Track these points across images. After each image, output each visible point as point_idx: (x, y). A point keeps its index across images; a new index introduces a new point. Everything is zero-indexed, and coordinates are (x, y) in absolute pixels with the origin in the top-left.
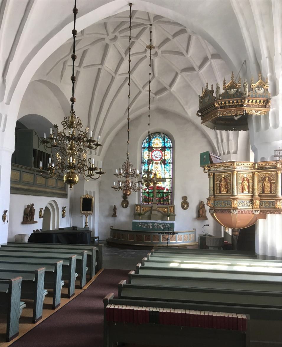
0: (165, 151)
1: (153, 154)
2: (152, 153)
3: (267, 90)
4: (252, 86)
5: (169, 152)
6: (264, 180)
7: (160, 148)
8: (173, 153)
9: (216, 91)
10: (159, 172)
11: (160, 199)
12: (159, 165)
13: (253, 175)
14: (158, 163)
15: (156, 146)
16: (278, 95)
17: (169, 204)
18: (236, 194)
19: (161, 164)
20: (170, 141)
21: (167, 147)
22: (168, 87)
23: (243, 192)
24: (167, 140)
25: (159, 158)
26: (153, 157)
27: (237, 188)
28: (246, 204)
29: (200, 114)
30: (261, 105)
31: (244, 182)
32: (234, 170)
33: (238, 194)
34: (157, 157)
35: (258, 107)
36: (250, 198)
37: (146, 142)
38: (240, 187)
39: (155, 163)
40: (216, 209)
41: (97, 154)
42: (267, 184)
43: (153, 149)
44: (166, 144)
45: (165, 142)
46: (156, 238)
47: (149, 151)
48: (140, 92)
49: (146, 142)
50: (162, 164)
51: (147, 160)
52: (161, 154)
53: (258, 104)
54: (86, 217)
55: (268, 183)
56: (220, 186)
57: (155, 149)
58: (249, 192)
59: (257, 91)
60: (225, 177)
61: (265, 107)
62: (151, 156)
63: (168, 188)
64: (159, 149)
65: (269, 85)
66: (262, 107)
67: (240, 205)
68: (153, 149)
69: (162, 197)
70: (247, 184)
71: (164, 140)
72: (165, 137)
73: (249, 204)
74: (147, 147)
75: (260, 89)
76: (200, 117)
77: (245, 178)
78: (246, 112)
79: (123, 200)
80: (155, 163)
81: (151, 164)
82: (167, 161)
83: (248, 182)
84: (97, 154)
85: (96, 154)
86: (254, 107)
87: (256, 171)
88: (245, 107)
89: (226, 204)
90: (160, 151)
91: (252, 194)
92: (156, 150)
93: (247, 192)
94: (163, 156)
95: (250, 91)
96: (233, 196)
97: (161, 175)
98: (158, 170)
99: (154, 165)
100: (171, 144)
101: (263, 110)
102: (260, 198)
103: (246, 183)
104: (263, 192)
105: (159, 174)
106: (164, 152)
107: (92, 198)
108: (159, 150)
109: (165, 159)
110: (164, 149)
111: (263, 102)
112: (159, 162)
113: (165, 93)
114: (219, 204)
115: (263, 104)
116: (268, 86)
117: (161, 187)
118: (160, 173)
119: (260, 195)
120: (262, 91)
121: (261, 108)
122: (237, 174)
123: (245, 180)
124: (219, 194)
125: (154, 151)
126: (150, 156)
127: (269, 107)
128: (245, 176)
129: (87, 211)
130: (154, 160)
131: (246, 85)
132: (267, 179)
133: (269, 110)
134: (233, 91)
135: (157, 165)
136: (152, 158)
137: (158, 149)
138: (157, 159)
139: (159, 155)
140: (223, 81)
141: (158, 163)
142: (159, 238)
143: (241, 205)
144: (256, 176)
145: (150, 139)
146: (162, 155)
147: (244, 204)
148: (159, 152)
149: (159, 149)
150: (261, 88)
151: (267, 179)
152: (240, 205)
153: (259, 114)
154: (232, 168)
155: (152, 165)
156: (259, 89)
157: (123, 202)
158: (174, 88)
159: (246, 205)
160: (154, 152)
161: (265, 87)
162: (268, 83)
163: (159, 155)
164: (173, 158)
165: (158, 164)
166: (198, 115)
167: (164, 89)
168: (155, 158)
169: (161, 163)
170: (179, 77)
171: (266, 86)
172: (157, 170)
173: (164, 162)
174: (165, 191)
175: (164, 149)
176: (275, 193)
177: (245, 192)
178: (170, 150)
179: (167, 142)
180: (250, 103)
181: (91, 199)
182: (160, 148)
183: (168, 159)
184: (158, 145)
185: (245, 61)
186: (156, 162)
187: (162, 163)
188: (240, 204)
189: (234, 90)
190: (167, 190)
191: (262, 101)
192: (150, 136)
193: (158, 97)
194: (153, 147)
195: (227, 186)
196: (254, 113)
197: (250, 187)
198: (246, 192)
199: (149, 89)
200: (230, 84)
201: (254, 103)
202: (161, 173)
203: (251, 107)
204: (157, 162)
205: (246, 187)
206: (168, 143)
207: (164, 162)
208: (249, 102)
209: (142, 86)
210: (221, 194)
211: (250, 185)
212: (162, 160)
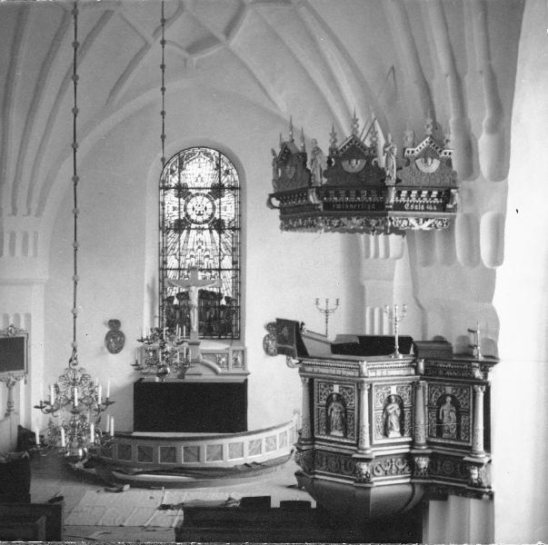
0: (220, 196)
1: (190, 206)
2: (188, 201)
3: (449, 162)
4: (406, 153)
5: (232, 200)
6: (441, 401)
7: (207, 188)
8: (240, 204)
9: (312, 161)
10: (207, 253)
11: (209, 324)
12: (206, 233)
13: (415, 385)
14: (203, 229)
15: (197, 185)
16: (440, 334)
17: (232, 336)
18: (367, 444)
19: (211, 232)
20: (235, 172)
21: (226, 185)
22: (222, 37)
23: (386, 434)
24: (225, 168)
25: (206, 217)
26: (190, 211)
27: (370, 428)
28: (394, 467)
29: (276, 202)
30: (433, 204)
31: (389, 407)
32: (363, 382)
33: (375, 442)
34: (199, 214)
35: (426, 210)
36: (405, 449)
37: (171, 173)
38: (378, 424)
39: (196, 229)
40: (317, 476)
41: (33, 213)
42: (448, 411)
43: (190, 193)
44: (223, 178)
45: (220, 172)
46: (190, 452)
47: (179, 196)
48: (147, 46)
49: (171, 173)
50: (215, 232)
51: (173, 222)
52: (209, 205)
53: (425, 200)
54: (10, 389)
55: (451, 411)
56: (327, 414)
57: (194, 192)
58: (402, 432)
59: (423, 168)
60: (341, 393)
61: (442, 208)
62: (185, 209)
63: (230, 295)
64: (206, 192)
65: (453, 150)
66: (435, 208)
67: (378, 471)
68: (190, 190)
69: (215, 318)
70: (398, 412)
71: (218, 167)
72: (220, 159)
73: (401, 467)
74: (173, 185)
75: (430, 161)
76: (277, 212)
77: (393, 397)
78: (392, 225)
79: (109, 332)
80: (196, 229)
81: (185, 232)
82: (227, 225)
83: (401, 407)
84: (33, 213)
85: (29, 213)
86: (414, 210)
87: (421, 379)
88: (390, 209)
89: (343, 467)
90: (207, 196)
91: (410, 439)
92: (197, 194)
93: (399, 435)
94: (217, 210)
95: (401, 168)
96: (360, 451)
97: (211, 262)
98: (203, 247)
99: (193, 233)
100: (237, 178)
101: (438, 216)
102: (430, 451)
103: (394, 408)
104: (440, 432)
105: (207, 259)
106: (218, 200)
107: (25, 336)
108: (205, 196)
109: (223, 218)
110: (217, 190)
111: (439, 196)
112: (206, 226)
113: (213, 51)
114: (324, 463)
115: (436, 201)
116: (450, 154)
117: (213, 293)
118: (208, 256)
119: (432, 440)
120: (434, 166)
121: (433, 211)
122: (370, 390)
123: (394, 401)
124: (325, 438)
125: (193, 196)
126: (182, 210)
127: (454, 209)
128: (394, 390)
129: (11, 372)
130: (192, 221)
131: (390, 150)
132: (449, 399)
133: (455, 216)
134: (356, 165)
135: (200, 235)
136: (187, 215)
137: (202, 192)
138: (200, 219)
139: (206, 208)
140: (331, 135)
141: (203, 229)
142: (199, 452)
143: (382, 472)
144: (420, 392)
145: (181, 163)
146: (214, 208)
147: (388, 468)
148: (206, 199)
149: (206, 192)
150: (432, 159)
151: (449, 399)
152: (378, 471)
153: (428, 229)
154: (357, 374)
155: (188, 233)
156: (426, 162)
157: (108, 336)
158: (236, 42)
159: (393, 472)
160: (193, 200)
161: (443, 155)
162: (450, 145)
163: (206, 208)
164: (240, 215)
165: (205, 232)
166: (269, 203)
167: (210, 40)
168: (194, 217)
169: (210, 229)
170: (249, 13)
171: (445, 153)
172: (199, 247)
173: (218, 225)
174: (223, 302)
175: (217, 190)
176: (468, 441)
177: (392, 434)
178: (235, 196)
179: (227, 172)
180: (403, 200)
181: (23, 338)
182: (207, 188)
183: (231, 219)
184: (202, 180)
185: (393, 68)
186: (198, 226)
187: (215, 229)
188: (379, 468)
189: (359, 162)
190: (228, 299)
191: (435, 193)
192: (181, 155)
193: (195, 59)
194: (190, 186)
195: (346, 416)
196: (412, 226)
197: (406, 418)
198: (395, 434)
199: (166, 46)
200: (348, 144)
201: (414, 200)
202: (212, 257)
203: (405, 210)
204: (202, 226)
205: (394, 420)
206: (229, 176)
207: (218, 225)
208: (399, 197)
209: (152, 32)
210: (329, 438)
211: (407, 414)
212: (213, 222)
